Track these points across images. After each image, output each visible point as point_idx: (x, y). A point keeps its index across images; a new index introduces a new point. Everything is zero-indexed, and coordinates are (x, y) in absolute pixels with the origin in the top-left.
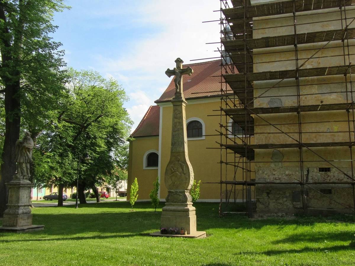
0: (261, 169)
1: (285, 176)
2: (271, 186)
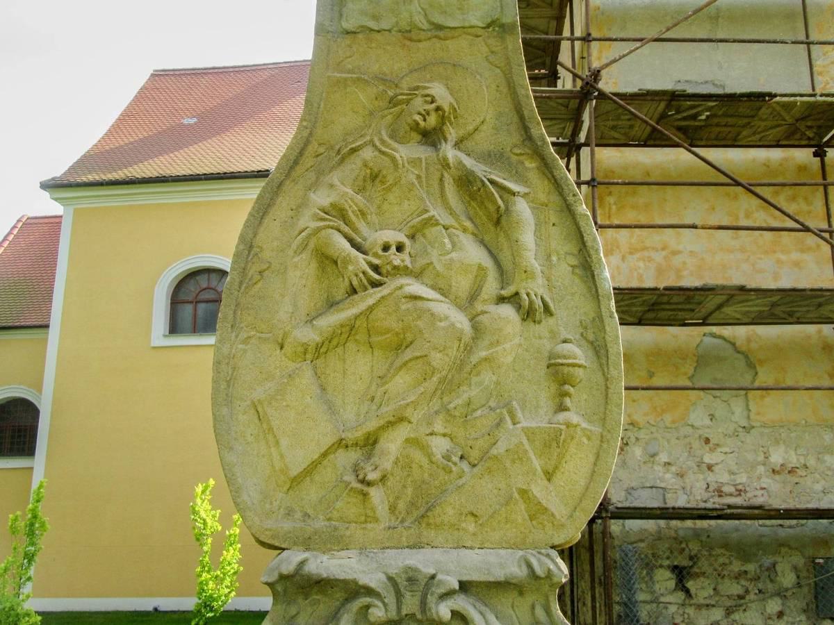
0: (637, 439)
1: (767, 477)
2: (697, 534)
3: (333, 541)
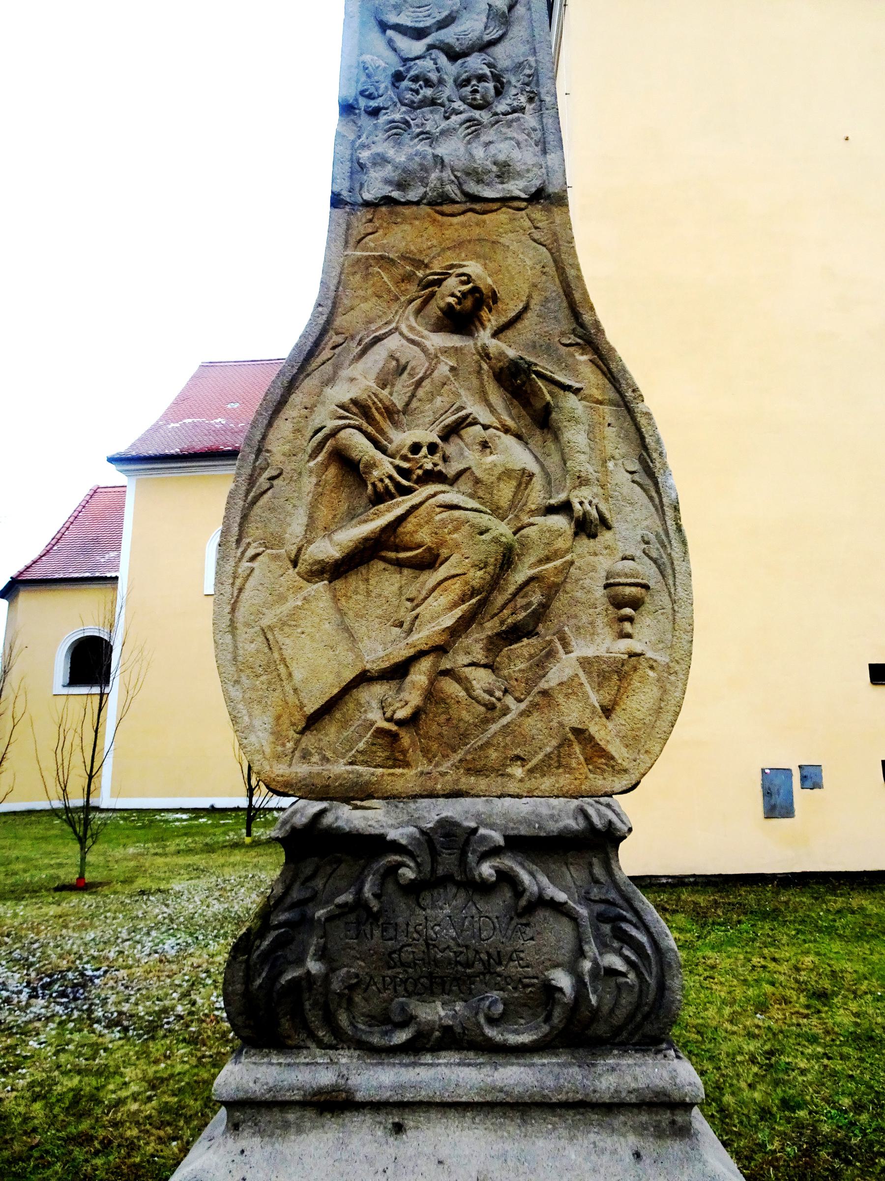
3: (357, 794)
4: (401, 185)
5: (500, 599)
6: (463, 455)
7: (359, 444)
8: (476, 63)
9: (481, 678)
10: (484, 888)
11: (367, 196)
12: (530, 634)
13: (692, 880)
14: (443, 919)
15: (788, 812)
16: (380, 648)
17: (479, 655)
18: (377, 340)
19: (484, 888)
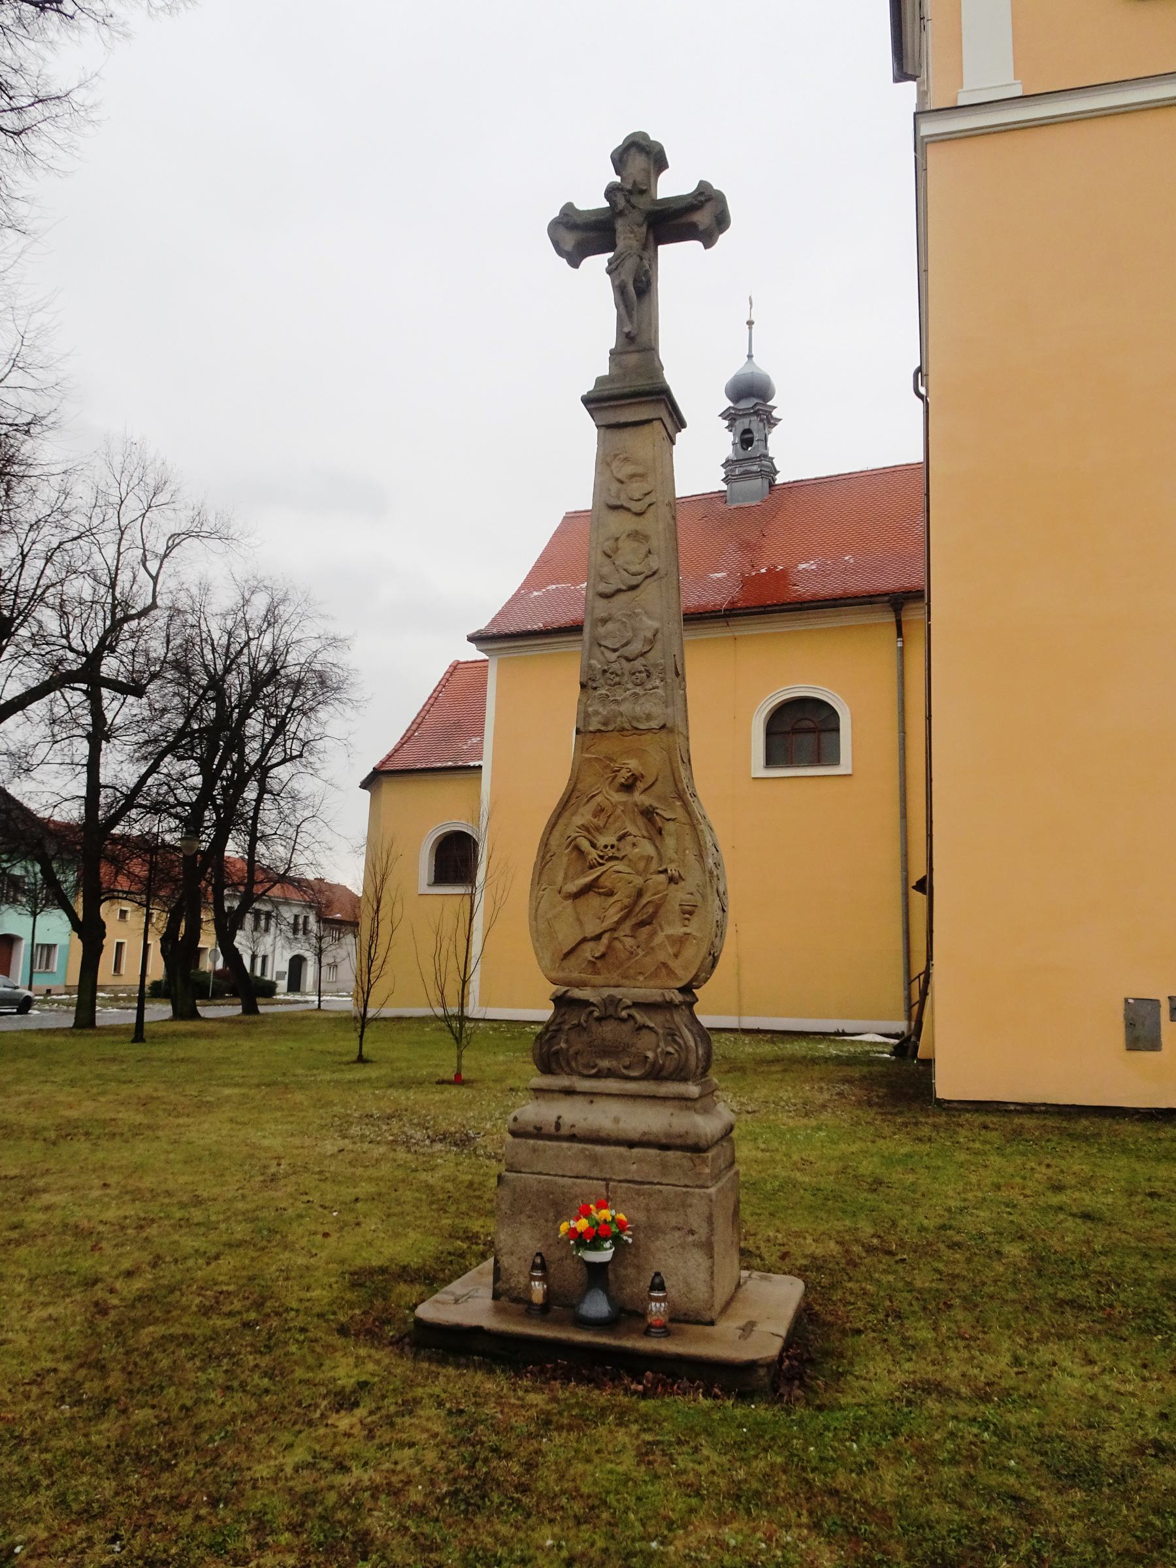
3: (581, 985)
4: (605, 724)
5: (637, 909)
6: (626, 849)
7: (585, 844)
8: (638, 664)
9: (629, 942)
10: (623, 1020)
11: (591, 729)
12: (650, 923)
13: (1043, 1108)
14: (609, 1031)
15: (1153, 1044)
16: (592, 929)
17: (628, 932)
18: (594, 796)
19: (623, 1020)
